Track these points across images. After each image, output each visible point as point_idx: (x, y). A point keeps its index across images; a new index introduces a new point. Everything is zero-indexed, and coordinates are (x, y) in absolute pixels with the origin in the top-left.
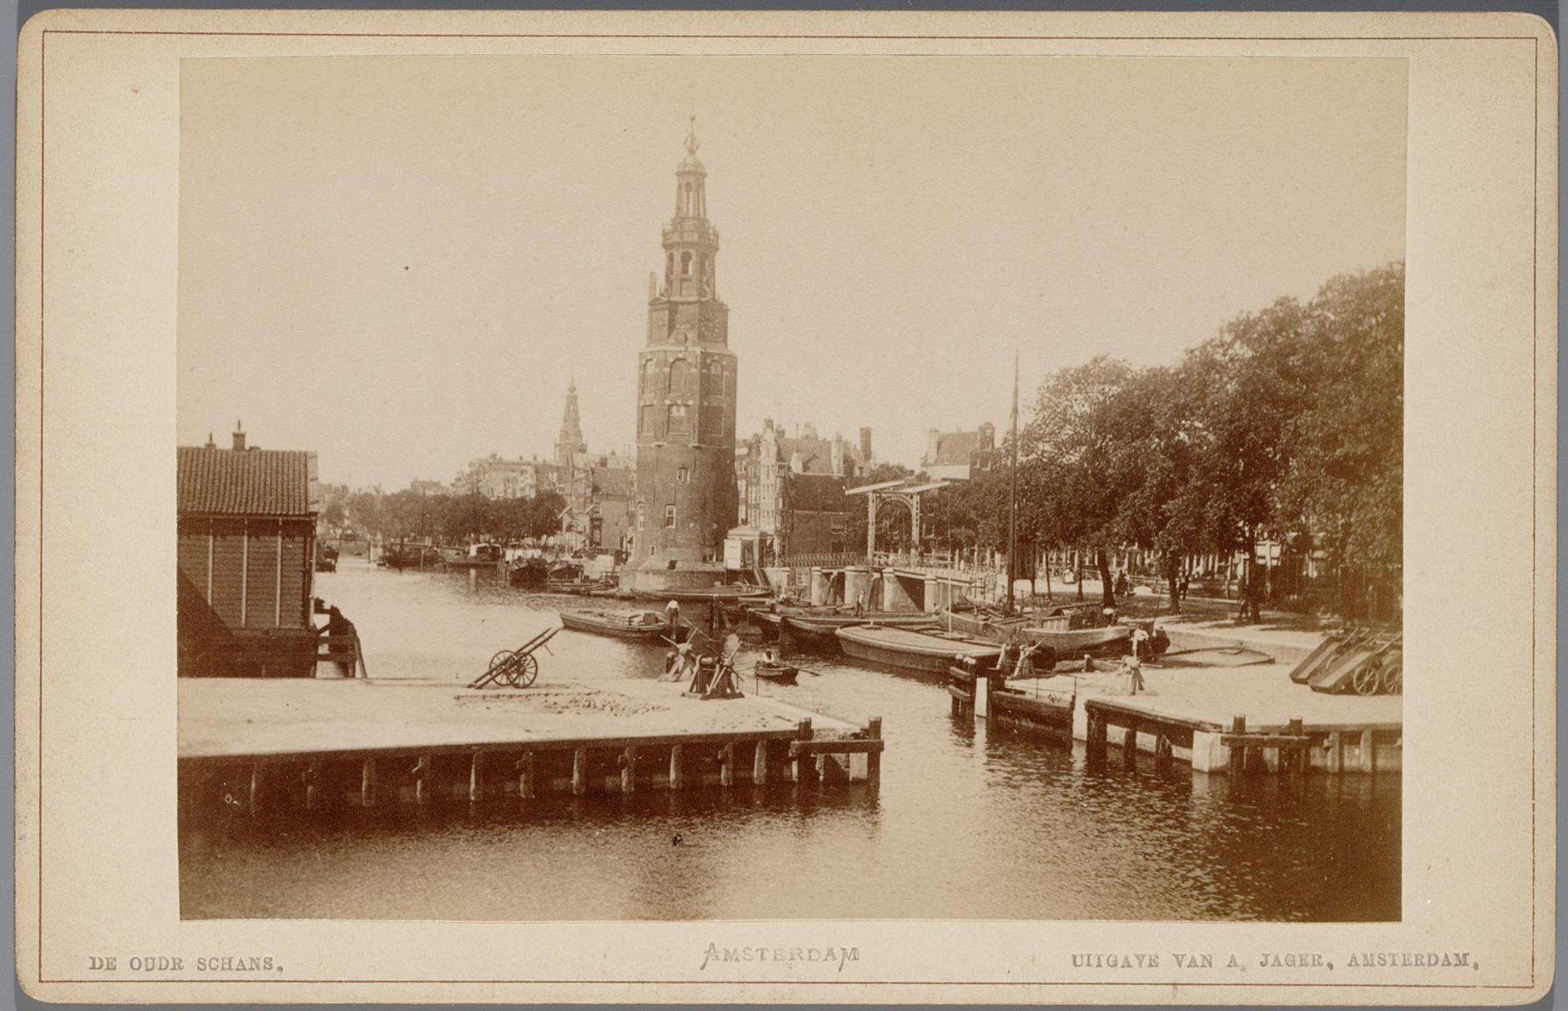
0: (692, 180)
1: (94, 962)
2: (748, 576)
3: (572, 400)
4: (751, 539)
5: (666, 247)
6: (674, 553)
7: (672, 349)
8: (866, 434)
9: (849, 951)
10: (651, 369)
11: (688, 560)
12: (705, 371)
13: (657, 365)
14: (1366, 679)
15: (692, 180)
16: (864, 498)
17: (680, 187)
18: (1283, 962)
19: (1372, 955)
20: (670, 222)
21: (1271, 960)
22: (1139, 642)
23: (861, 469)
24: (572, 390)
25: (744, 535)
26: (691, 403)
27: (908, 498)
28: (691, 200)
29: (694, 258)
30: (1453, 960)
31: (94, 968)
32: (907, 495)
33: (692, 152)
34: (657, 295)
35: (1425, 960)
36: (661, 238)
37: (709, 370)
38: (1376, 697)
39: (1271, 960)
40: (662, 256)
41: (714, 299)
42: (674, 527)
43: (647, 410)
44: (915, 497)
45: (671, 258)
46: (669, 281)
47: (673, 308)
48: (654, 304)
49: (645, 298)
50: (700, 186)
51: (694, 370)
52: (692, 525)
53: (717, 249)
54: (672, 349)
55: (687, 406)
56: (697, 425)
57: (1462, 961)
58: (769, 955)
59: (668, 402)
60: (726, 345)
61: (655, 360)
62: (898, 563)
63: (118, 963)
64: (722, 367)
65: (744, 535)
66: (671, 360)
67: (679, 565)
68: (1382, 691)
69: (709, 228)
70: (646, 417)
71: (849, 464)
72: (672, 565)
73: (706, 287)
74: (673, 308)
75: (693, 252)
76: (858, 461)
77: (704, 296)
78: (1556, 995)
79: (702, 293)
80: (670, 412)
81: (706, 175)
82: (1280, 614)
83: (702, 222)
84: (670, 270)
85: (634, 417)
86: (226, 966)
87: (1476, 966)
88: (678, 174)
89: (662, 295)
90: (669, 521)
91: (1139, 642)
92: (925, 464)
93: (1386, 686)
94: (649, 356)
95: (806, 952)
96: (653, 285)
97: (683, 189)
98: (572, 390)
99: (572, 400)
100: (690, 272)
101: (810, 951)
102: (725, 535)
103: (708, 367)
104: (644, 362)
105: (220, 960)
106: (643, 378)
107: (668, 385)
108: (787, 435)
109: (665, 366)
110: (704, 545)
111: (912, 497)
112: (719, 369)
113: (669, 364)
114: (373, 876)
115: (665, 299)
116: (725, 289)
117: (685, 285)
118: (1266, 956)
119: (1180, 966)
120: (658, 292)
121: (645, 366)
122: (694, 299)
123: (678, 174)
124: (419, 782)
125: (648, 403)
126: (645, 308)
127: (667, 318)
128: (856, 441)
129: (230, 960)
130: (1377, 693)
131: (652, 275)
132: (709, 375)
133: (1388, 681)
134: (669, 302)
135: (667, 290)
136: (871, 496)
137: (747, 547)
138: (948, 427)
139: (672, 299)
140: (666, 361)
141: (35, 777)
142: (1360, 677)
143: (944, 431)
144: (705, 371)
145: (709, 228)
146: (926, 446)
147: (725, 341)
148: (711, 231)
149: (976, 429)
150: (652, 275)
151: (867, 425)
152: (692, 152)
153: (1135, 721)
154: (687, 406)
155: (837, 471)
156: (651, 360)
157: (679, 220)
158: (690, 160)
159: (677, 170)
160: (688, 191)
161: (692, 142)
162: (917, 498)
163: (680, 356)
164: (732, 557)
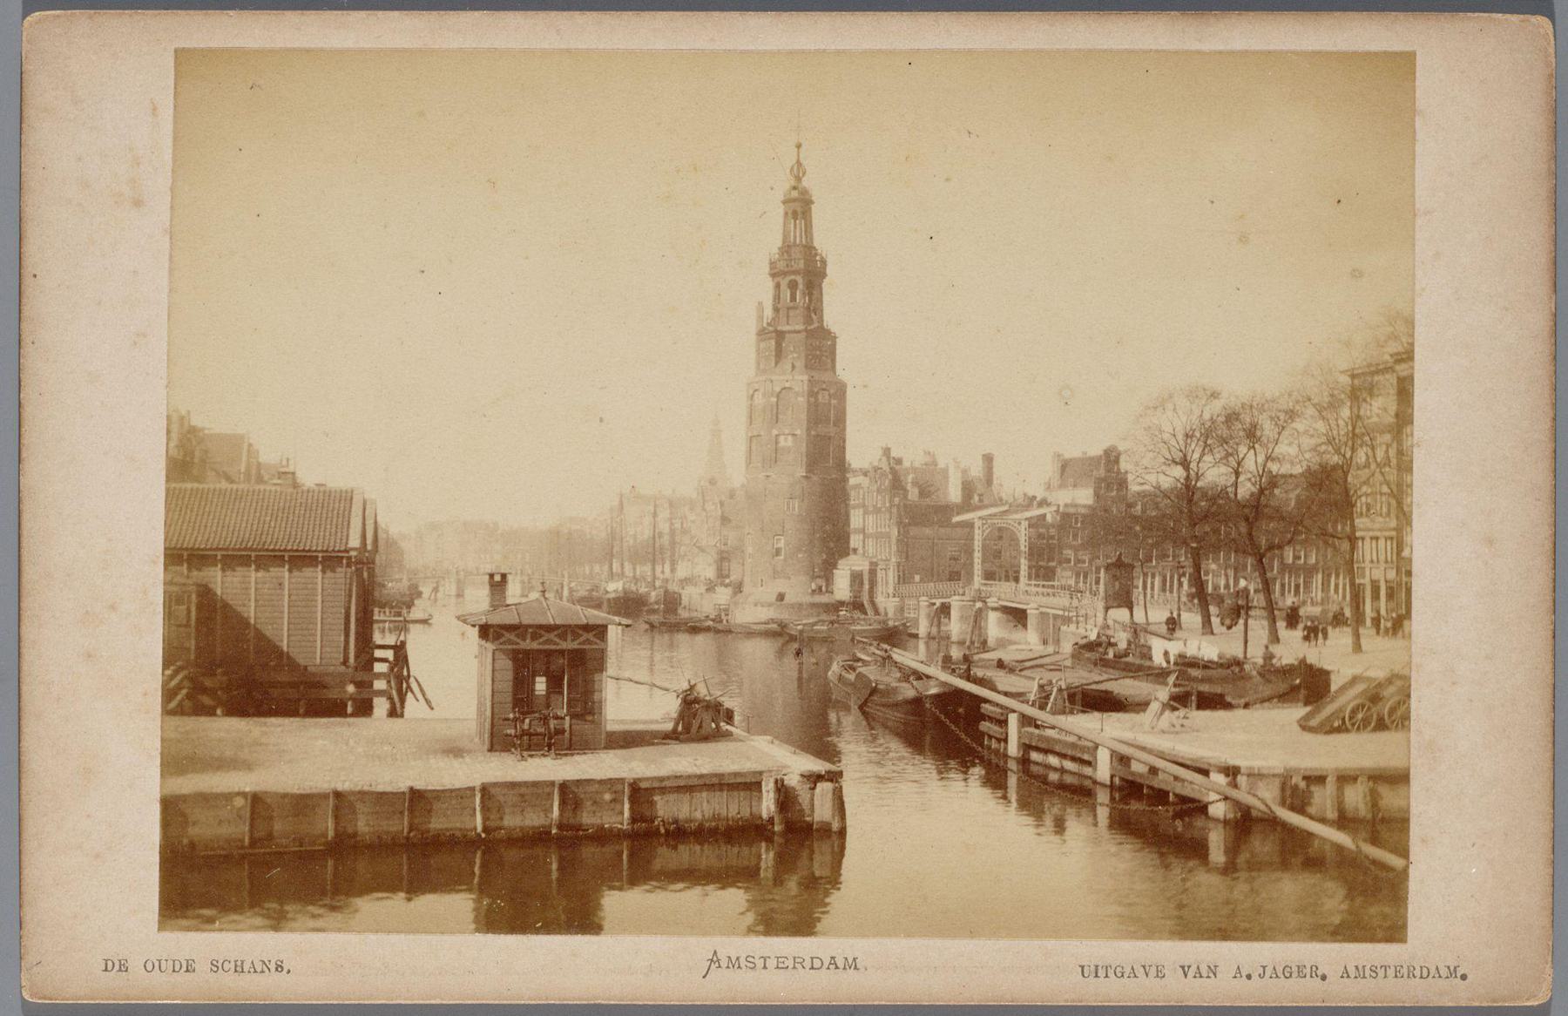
0: (800, 207)
1: (106, 964)
4: (860, 568)
5: (773, 275)
6: (780, 586)
8: (988, 459)
9: (850, 961)
10: (759, 400)
11: (798, 589)
13: (764, 395)
14: (1360, 716)
15: (800, 207)
16: (969, 525)
17: (786, 214)
18: (1280, 974)
19: (1364, 967)
20: (777, 251)
21: (1269, 971)
23: (980, 495)
25: (853, 565)
26: (798, 432)
27: (1016, 525)
28: (798, 226)
29: (801, 286)
30: (1444, 972)
31: (106, 970)
32: (1015, 520)
33: (799, 179)
34: (765, 325)
35: (1417, 973)
38: (1371, 735)
39: (1269, 971)
41: (822, 327)
42: (782, 557)
43: (754, 440)
44: (1023, 522)
45: (778, 286)
46: (776, 310)
47: (780, 335)
48: (762, 333)
49: (753, 328)
51: (801, 399)
52: (800, 556)
55: (794, 435)
57: (1453, 972)
58: (772, 963)
59: (775, 432)
60: (835, 373)
61: (762, 390)
62: (1003, 592)
63: (130, 964)
65: (853, 565)
66: (778, 389)
67: (787, 599)
68: (1381, 726)
69: (816, 255)
70: (754, 448)
71: (968, 488)
72: (781, 597)
73: (813, 315)
74: (780, 335)
76: (979, 487)
77: (810, 325)
78: (1553, 1003)
79: (808, 320)
80: (777, 443)
81: (812, 202)
82: (1089, 687)
83: (809, 250)
84: (777, 298)
85: (743, 448)
86: (239, 969)
87: (1464, 977)
89: (768, 324)
90: (778, 552)
92: (1048, 487)
93: (1387, 721)
95: (1418, 969)
96: (760, 318)
101: (812, 958)
102: (835, 566)
104: (751, 392)
105: (233, 963)
106: (751, 409)
107: (776, 415)
108: (906, 464)
109: (772, 395)
110: (813, 578)
111: (1020, 524)
112: (827, 397)
115: (771, 329)
117: (792, 313)
118: (1264, 967)
119: (1186, 976)
120: (765, 321)
121: (753, 396)
122: (800, 327)
123: (784, 202)
126: (753, 338)
127: (773, 347)
128: (977, 470)
129: (242, 962)
130: (1375, 729)
131: (760, 304)
132: (816, 405)
133: (1350, 718)
134: (776, 331)
135: (773, 319)
136: (978, 523)
137: (856, 578)
138: (1073, 452)
139: (779, 328)
142: (1354, 712)
143: (1067, 456)
145: (816, 255)
146: (1050, 470)
147: (833, 368)
149: (1100, 452)
150: (760, 304)
151: (988, 451)
154: (794, 435)
155: (954, 494)
157: (786, 249)
160: (795, 219)
161: (798, 169)
162: (1025, 524)
163: (787, 385)
164: (842, 588)
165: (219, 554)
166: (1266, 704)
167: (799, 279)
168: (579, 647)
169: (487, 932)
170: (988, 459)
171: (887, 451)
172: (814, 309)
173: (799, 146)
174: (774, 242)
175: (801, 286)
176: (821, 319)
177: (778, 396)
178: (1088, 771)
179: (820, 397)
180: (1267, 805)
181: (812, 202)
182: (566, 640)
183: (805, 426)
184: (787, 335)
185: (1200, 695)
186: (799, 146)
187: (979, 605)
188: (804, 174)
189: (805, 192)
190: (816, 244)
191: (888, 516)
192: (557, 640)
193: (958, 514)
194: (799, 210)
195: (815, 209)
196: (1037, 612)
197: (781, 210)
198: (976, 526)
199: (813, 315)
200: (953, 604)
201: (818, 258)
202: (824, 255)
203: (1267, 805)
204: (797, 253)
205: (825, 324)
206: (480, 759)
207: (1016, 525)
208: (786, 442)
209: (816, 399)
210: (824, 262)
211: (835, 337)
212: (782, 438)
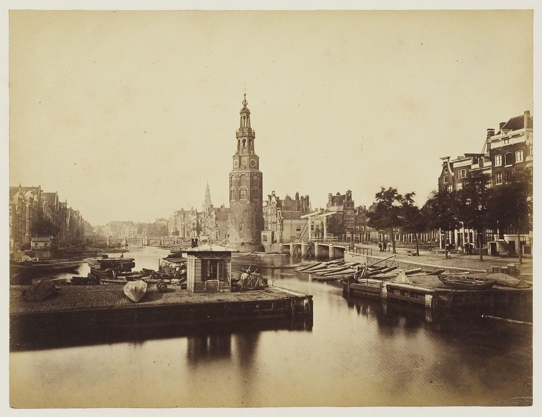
0: (246, 113)
3: (208, 190)
15: (246, 113)
24: (208, 187)
29: (247, 141)
33: (245, 105)
40: (236, 141)
42: (243, 231)
44: (324, 217)
45: (239, 141)
53: (255, 138)
59: (239, 189)
61: (235, 176)
66: (240, 175)
69: (252, 131)
73: (251, 151)
80: (240, 193)
81: (250, 113)
83: (250, 129)
94: (233, 174)
98: (208, 187)
99: (208, 190)
100: (246, 146)
104: (231, 176)
106: (231, 182)
111: (323, 218)
116: (257, 152)
122: (247, 155)
136: (309, 218)
145: (252, 131)
146: (327, 200)
148: (252, 132)
156: (233, 175)
157: (241, 129)
159: (240, 112)
165: (379, 235)
167: (246, 138)
169: (11, 317)
172: (251, 147)
175: (247, 141)
177: (240, 178)
179: (254, 178)
181: (250, 113)
183: (249, 187)
184: (243, 157)
185: (468, 279)
186: (245, 95)
188: (247, 104)
190: (251, 127)
191: (276, 216)
196: (332, 247)
199: (251, 151)
200: (290, 245)
201: (252, 132)
204: (246, 130)
206: (439, 363)
207: (322, 218)
209: (253, 178)
210: (254, 133)
211: (258, 158)
212: (242, 191)
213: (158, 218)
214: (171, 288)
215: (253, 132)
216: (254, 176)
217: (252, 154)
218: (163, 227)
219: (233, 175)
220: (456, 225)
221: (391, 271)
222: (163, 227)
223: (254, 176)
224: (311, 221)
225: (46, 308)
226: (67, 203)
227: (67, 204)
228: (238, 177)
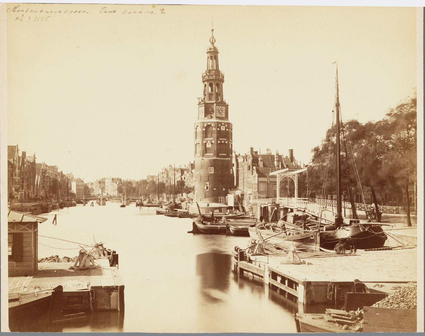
2: (237, 208)
5: (204, 82)
7: (208, 120)
8: (291, 151)
12: (218, 129)
16: (275, 177)
22: (294, 197)
36: (201, 78)
37: (220, 129)
43: (197, 145)
44: (295, 175)
50: (216, 58)
53: (223, 81)
54: (208, 120)
56: (216, 150)
61: (200, 126)
64: (225, 127)
66: (205, 125)
75: (213, 83)
79: (217, 99)
81: (218, 53)
83: (217, 71)
88: (207, 53)
91: (294, 197)
97: (210, 58)
103: (220, 128)
104: (196, 127)
108: (258, 154)
111: (294, 176)
112: (224, 128)
113: (205, 127)
114: (192, 200)
121: (196, 128)
124: (225, 155)
125: (198, 143)
128: (288, 154)
140: (204, 126)
141: (256, 184)
144: (218, 129)
152: (213, 44)
153: (116, 292)
156: (198, 126)
158: (212, 47)
159: (207, 51)
160: (212, 59)
166: (220, 251)
168: (20, 232)
170: (291, 151)
171: (252, 149)
172: (219, 95)
173: (213, 30)
174: (204, 69)
176: (222, 98)
178: (262, 279)
179: (222, 128)
180: (394, 287)
181: (218, 53)
182: (14, 229)
183: (216, 139)
186: (213, 30)
187: (276, 208)
188: (215, 41)
189: (215, 48)
192: (27, 228)
193: (272, 172)
194: (213, 56)
195: (219, 56)
197: (207, 55)
198: (277, 176)
202: (223, 73)
203: (394, 287)
205: (224, 100)
208: (209, 146)
213: (149, 175)
214: (329, 309)
215: (222, 74)
216: (222, 126)
217: (220, 100)
218: (382, 173)
219: (198, 126)
220: (216, 190)
221: (37, 215)
222: (382, 173)
223: (222, 126)
224: (279, 179)
225: (16, 304)
226: (35, 157)
227: (36, 158)
228: (204, 128)
